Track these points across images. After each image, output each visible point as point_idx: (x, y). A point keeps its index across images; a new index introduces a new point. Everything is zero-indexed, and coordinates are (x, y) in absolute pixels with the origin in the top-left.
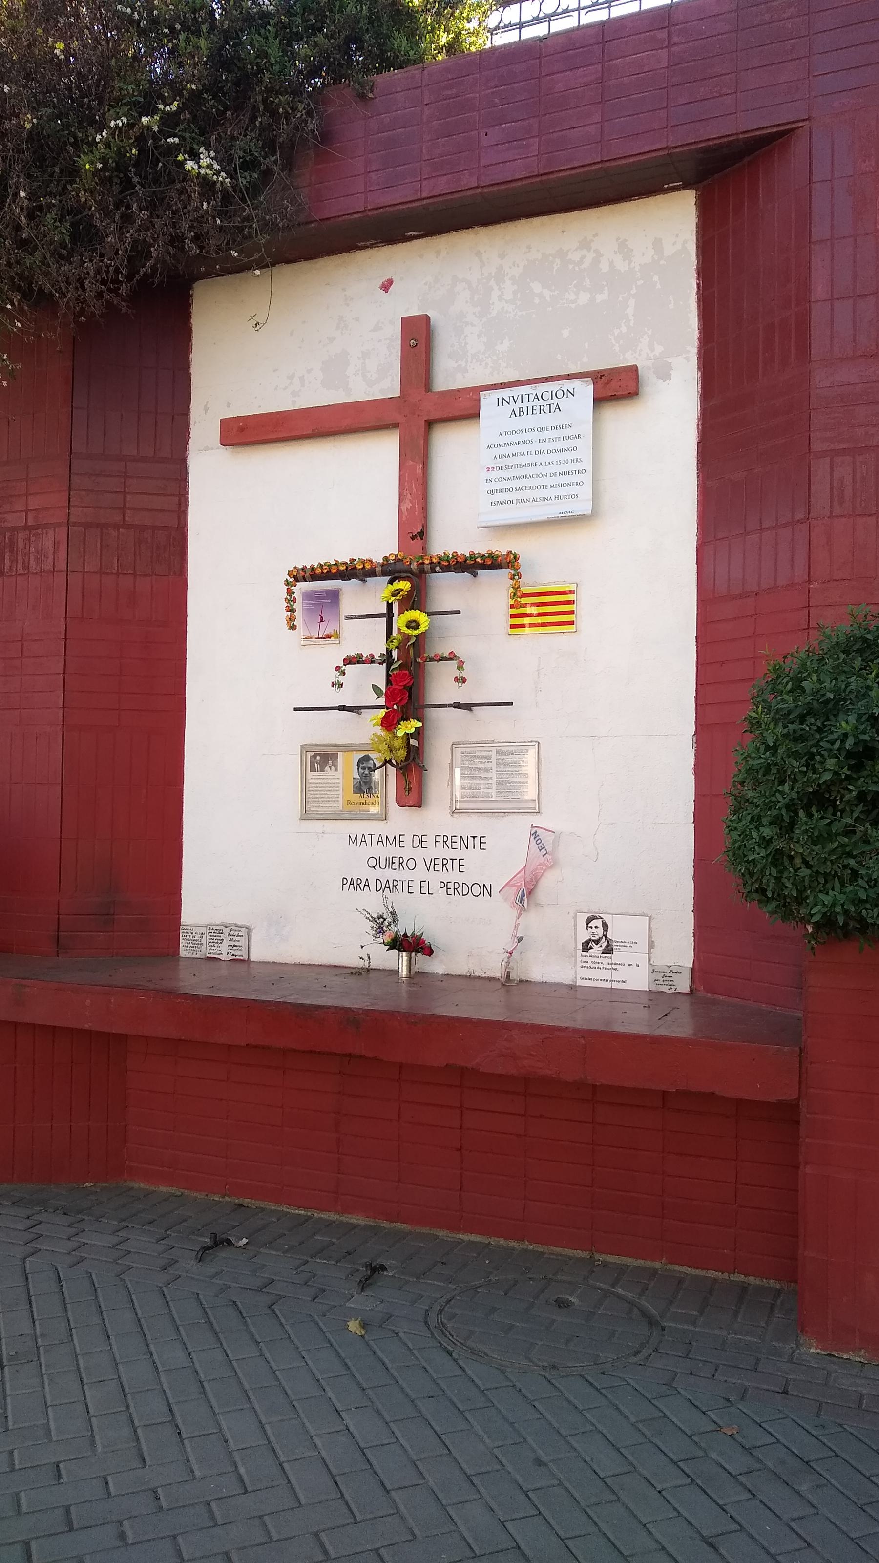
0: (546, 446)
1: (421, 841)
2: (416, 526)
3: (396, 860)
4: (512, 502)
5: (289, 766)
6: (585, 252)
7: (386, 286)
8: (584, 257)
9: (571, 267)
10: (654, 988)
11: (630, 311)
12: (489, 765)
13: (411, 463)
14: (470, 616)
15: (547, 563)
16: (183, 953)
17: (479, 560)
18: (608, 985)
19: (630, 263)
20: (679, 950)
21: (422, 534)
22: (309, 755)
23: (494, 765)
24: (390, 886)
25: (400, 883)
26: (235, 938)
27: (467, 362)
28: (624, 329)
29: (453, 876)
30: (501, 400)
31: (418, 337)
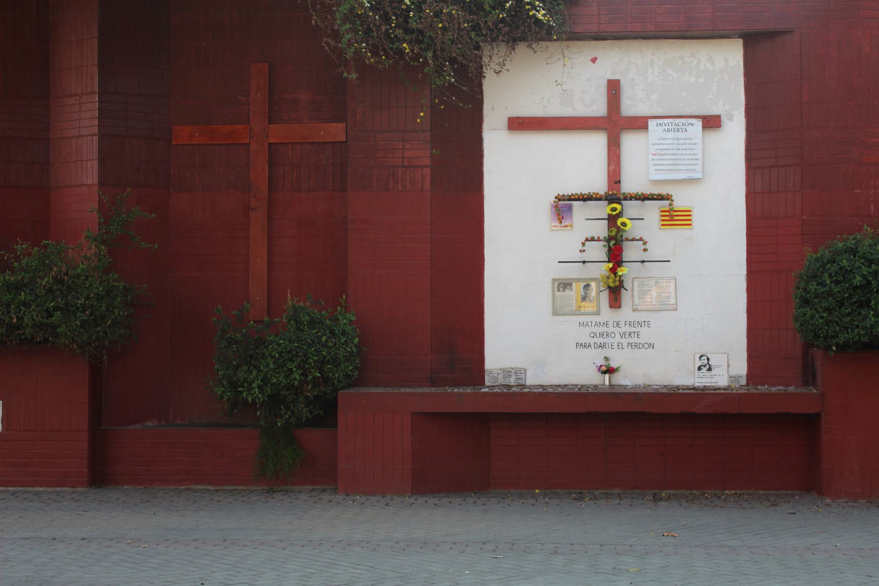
0: (680, 147)
2: (614, 179)
5: (547, 288)
7: (594, 60)
14: (642, 222)
15: (681, 201)
20: (740, 367)
21: (619, 182)
24: (602, 346)
29: (634, 340)
31: (614, 89)
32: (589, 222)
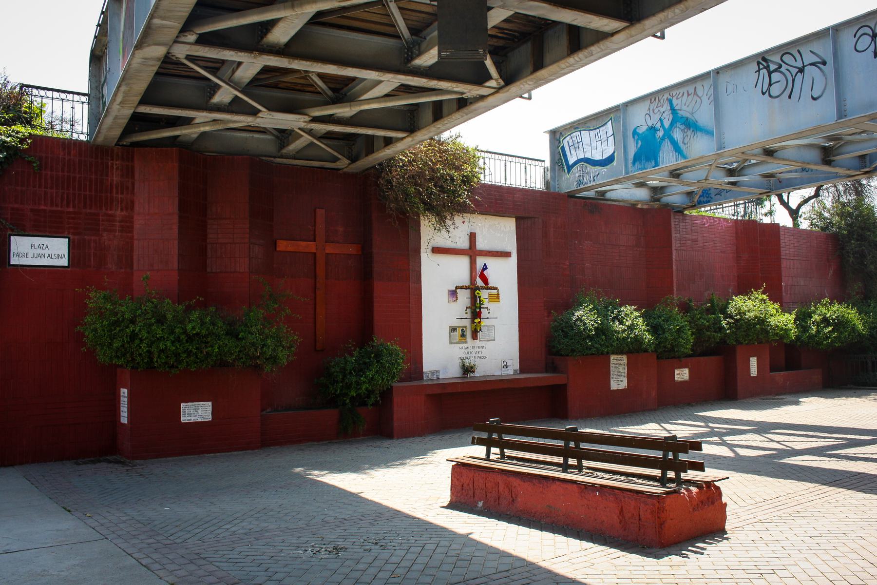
2: (466, 288)
5: (447, 331)
20: (517, 366)
31: (472, 237)
32: (464, 297)
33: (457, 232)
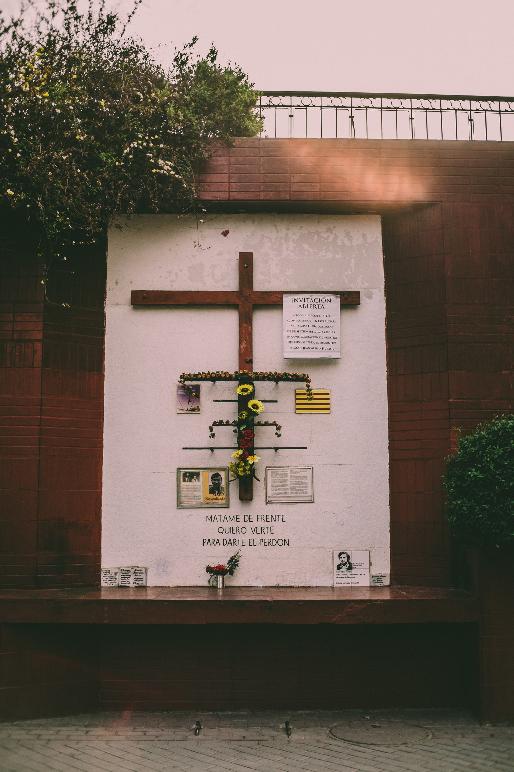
1: (249, 518)
2: (246, 357)
3: (235, 529)
4: (301, 348)
6: (329, 234)
8: (329, 236)
9: (323, 240)
10: (373, 585)
11: (352, 265)
12: (287, 478)
13: (246, 325)
15: (319, 380)
16: (103, 584)
17: (289, 377)
18: (350, 585)
19: (352, 242)
20: (383, 567)
22: (182, 473)
23: (289, 478)
24: (231, 543)
25: (237, 541)
26: (138, 574)
27: (270, 277)
28: (350, 273)
29: (267, 536)
30: (293, 300)
31: (246, 262)
32: (218, 404)
33: (201, 256)
